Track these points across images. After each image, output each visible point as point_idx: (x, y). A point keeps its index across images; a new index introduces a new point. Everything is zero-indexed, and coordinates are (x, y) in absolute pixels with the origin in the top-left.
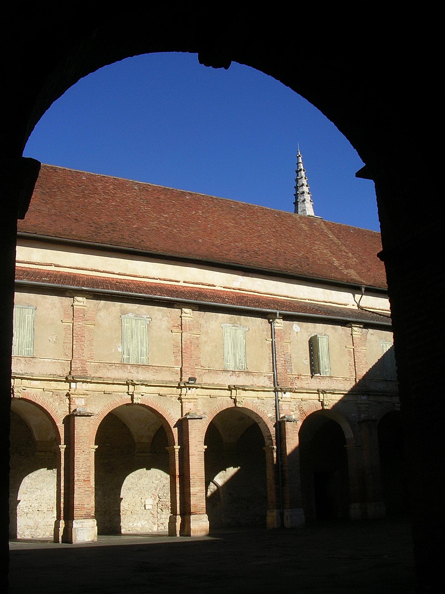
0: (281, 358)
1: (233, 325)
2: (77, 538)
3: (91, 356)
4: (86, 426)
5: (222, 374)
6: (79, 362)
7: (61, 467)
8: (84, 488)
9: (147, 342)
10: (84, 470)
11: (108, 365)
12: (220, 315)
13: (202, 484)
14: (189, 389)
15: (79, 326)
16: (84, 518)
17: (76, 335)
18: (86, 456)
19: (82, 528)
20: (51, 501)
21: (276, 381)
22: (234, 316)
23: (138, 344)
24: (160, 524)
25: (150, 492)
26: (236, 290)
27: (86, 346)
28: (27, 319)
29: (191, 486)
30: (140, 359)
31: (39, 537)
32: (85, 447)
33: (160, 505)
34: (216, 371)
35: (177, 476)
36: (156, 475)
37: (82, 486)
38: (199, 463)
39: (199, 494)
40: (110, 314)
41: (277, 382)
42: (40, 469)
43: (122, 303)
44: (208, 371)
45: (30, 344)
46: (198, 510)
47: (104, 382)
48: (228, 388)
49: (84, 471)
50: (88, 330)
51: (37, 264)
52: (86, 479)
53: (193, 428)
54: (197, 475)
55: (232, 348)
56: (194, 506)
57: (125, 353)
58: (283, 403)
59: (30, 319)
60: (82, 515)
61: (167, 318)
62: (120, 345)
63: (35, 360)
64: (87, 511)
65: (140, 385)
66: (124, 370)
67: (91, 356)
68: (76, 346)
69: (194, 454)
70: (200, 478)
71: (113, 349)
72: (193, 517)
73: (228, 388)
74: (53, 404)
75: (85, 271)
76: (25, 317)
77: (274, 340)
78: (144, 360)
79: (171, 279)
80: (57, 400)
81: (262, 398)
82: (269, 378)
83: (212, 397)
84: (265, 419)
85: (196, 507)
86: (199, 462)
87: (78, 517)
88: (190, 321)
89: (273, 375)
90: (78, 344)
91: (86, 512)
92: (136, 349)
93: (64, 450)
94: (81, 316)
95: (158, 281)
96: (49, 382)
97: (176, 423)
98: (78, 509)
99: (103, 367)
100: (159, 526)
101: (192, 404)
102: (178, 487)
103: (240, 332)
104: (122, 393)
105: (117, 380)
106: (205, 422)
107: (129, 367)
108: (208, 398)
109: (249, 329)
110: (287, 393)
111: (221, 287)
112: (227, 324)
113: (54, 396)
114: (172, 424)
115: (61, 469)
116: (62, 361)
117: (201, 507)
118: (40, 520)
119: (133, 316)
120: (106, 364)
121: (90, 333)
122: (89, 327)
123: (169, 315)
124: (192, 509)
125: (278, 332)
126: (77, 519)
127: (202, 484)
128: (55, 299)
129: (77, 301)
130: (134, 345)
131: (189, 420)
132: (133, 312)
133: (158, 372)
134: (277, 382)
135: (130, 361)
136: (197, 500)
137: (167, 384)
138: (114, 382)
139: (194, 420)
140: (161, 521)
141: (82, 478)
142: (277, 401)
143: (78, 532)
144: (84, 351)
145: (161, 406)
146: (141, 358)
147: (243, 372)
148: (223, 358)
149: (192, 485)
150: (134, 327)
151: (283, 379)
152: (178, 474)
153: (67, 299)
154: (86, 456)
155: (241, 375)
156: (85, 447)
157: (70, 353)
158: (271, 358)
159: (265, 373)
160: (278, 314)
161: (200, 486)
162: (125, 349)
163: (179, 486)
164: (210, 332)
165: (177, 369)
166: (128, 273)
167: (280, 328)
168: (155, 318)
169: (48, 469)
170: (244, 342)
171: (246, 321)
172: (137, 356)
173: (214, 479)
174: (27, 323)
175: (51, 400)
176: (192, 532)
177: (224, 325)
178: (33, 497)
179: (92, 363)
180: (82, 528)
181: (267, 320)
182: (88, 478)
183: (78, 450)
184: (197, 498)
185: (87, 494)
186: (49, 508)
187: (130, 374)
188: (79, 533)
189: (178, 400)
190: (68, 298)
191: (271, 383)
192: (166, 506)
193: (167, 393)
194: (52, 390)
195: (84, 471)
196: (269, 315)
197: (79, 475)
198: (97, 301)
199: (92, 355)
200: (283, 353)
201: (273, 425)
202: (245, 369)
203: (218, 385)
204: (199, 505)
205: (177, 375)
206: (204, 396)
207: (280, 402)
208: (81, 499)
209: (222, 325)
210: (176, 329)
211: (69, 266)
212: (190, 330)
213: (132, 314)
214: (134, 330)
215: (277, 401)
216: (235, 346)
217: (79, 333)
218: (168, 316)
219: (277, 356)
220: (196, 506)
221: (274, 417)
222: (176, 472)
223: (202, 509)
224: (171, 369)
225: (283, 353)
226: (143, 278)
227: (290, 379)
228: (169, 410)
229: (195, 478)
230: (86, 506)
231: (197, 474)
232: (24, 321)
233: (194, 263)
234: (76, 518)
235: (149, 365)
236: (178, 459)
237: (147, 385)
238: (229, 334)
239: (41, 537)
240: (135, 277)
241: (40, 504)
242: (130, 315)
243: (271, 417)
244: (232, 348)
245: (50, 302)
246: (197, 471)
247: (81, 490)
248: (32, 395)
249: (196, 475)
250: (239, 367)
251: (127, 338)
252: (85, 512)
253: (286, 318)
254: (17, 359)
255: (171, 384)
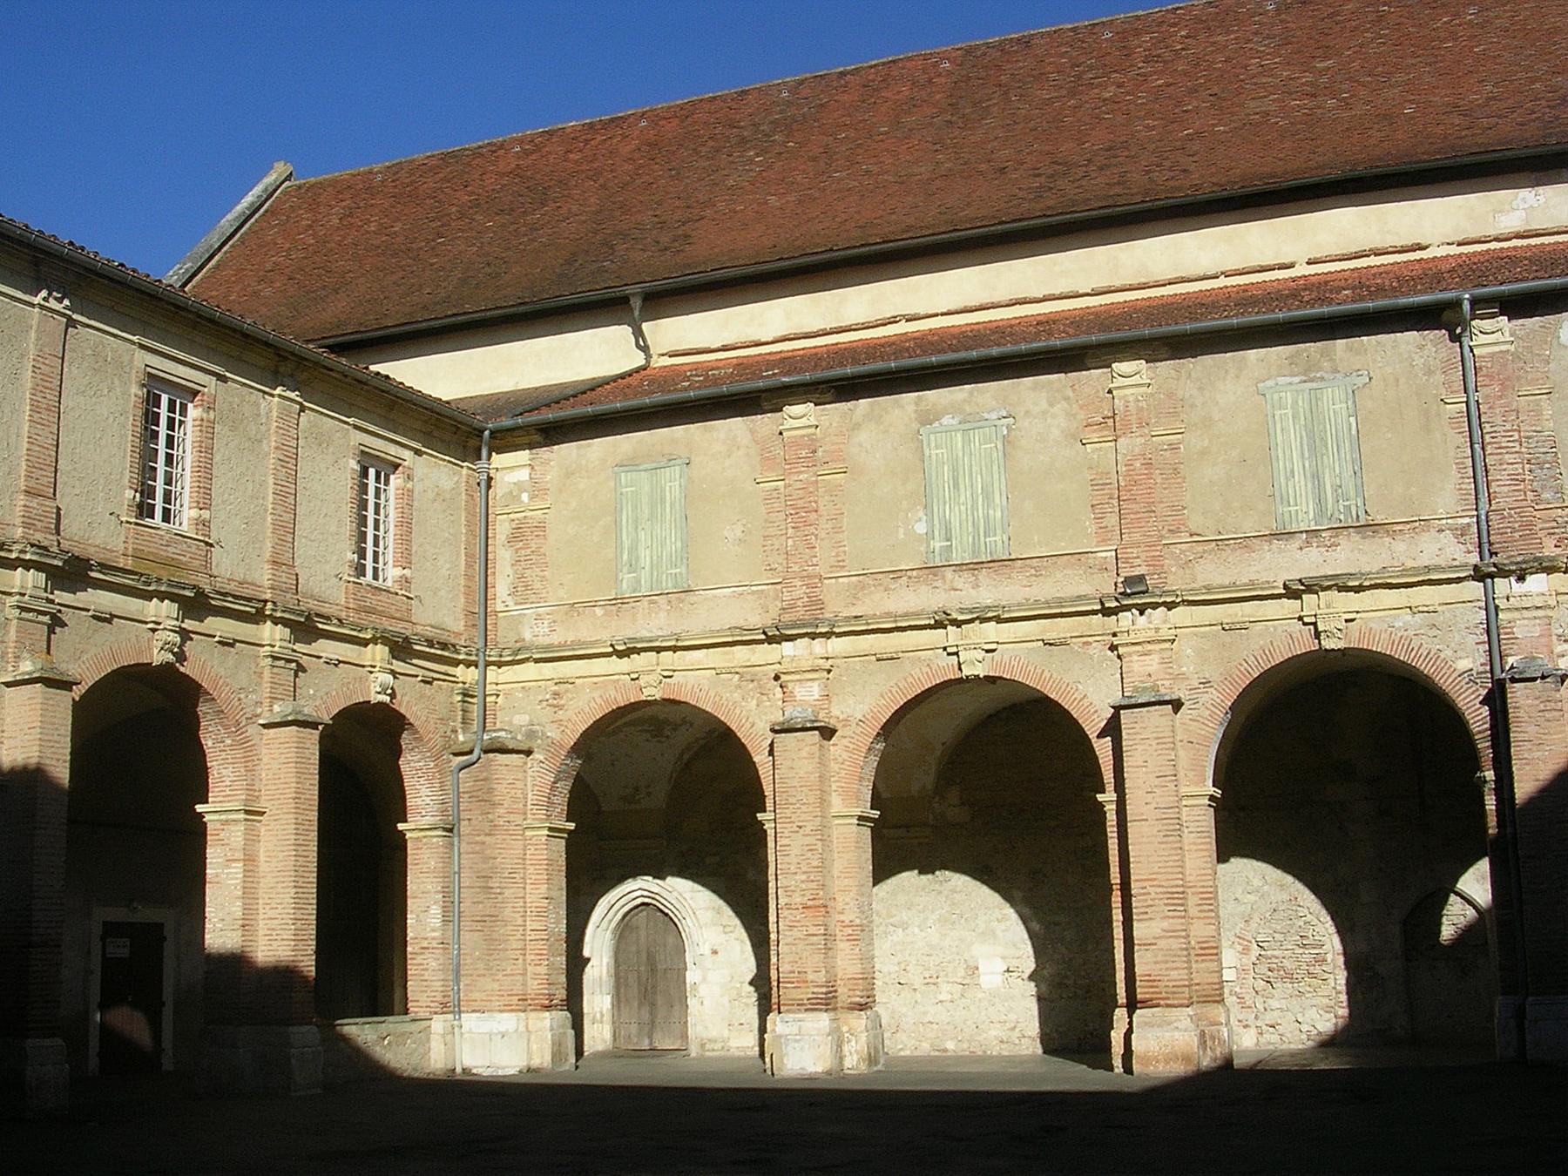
0: (1507, 456)
1: (1304, 378)
2: (785, 1062)
3: (839, 561)
4: (805, 758)
5: (1266, 548)
6: (800, 583)
7: (770, 872)
8: (804, 928)
9: (1004, 488)
10: (804, 877)
11: (886, 579)
12: (1253, 355)
13: (1175, 910)
14: (1142, 613)
15: (799, 485)
16: (806, 1010)
17: (793, 512)
18: (808, 840)
19: (798, 1037)
20: (933, 958)
21: (1485, 540)
22: (1308, 345)
23: (975, 502)
24: (1264, 1027)
25: (1229, 930)
26: (1510, 239)
27: (823, 534)
28: (668, 494)
29: (1135, 917)
30: (982, 543)
31: (902, 1053)
32: (804, 817)
33: (1263, 969)
34: (1244, 542)
35: (1114, 887)
36: (1247, 877)
37: (799, 921)
38: (1163, 846)
39: (1162, 943)
40: (887, 431)
41: (1490, 544)
42: (900, 872)
43: (921, 393)
44: (1214, 543)
45: (679, 559)
46: (1161, 993)
47: (870, 627)
48: (1284, 592)
49: (803, 882)
50: (826, 491)
51: (859, 326)
52: (810, 903)
53: (1139, 737)
54: (1155, 883)
55: (1306, 455)
56: (1148, 981)
57: (936, 533)
58: (1516, 615)
59: (677, 492)
60: (802, 1000)
61: (1066, 405)
62: (921, 514)
63: (690, 597)
64: (815, 990)
65: (977, 622)
66: (935, 584)
67: (839, 561)
68: (794, 541)
69: (1144, 817)
70: (1165, 893)
71: (901, 531)
72: (1142, 1016)
73: (1284, 592)
74: (741, 706)
75: (992, 310)
76: (663, 490)
77: (1474, 397)
78: (997, 545)
79: (1263, 264)
80: (751, 693)
81: (1426, 609)
82: (1462, 532)
83: (1227, 627)
84: (1445, 682)
85: (1155, 984)
86: (1162, 843)
87: (789, 1005)
88: (1140, 398)
89: (1475, 519)
90: (798, 534)
91: (813, 993)
92: (970, 518)
93: (1114, 807)
94: (804, 455)
95: (1222, 282)
96: (728, 648)
97: (1105, 721)
98: (789, 985)
99: (874, 585)
100: (1261, 1034)
101: (1156, 658)
102: (1117, 921)
103: (1334, 399)
104: (931, 652)
105: (906, 615)
106: (1208, 712)
107: (949, 573)
108: (1217, 631)
109: (1370, 379)
110: (1529, 578)
111: (1448, 244)
112: (1281, 380)
113: (745, 683)
114: (1092, 727)
115: (770, 878)
116: (760, 588)
117: (1171, 984)
118: (904, 1010)
119: (955, 422)
120: (880, 576)
121: (832, 498)
122: (829, 481)
123: (1071, 394)
124: (1138, 990)
125: (1489, 365)
126: (788, 1011)
127: (1175, 910)
128: (735, 426)
129: (790, 417)
130: (963, 508)
131: (1122, 712)
132: (954, 409)
133: (1041, 575)
134: (1490, 544)
135: (954, 555)
136: (1156, 963)
137: (1063, 607)
138: (899, 624)
139: (1150, 708)
140: (1269, 1018)
141: (798, 900)
142: (1492, 610)
143: (787, 1045)
144: (817, 550)
145: (1055, 675)
146: (988, 540)
147: (1351, 530)
148: (1269, 493)
149: (1138, 914)
150: (960, 454)
151: (1514, 530)
152: (1119, 882)
153: (766, 419)
154: (808, 840)
155: (1342, 540)
156: (804, 817)
157: (780, 561)
158: (1469, 462)
159: (1439, 519)
160: (1466, 306)
161: (1168, 917)
162: (936, 522)
163: (1121, 918)
164: (1216, 416)
165: (1104, 554)
166: (1118, 283)
167: (1496, 349)
168: (1027, 412)
169: (920, 873)
170: (1354, 425)
171: (1358, 353)
172: (974, 539)
173: (1458, 886)
174: (668, 505)
175: (736, 695)
176: (1137, 1062)
177: (1270, 383)
178: (884, 948)
179: (841, 580)
180: (798, 1037)
181: (1444, 331)
182: (814, 899)
183: (785, 825)
184: (1156, 956)
185: (812, 944)
186: (927, 976)
187: (952, 592)
188: (789, 1048)
189: (1109, 652)
190: (769, 415)
191: (1469, 552)
192: (1282, 972)
193: (1069, 635)
194: (737, 670)
195: (803, 882)
196: (1445, 313)
197: (789, 892)
198: (849, 404)
199: (840, 559)
200: (1517, 437)
201: (1481, 698)
202: (1358, 516)
203: (1252, 584)
204: (1166, 978)
205: (1105, 575)
206: (1202, 629)
207: (1501, 616)
208: (798, 956)
209: (1260, 385)
210: (1095, 431)
211: (945, 310)
212: (1140, 426)
213: (953, 418)
214: (961, 462)
215: (1492, 610)
216: (1314, 444)
217: (800, 503)
218: (1067, 399)
219: (1489, 450)
220: (1154, 981)
221: (1481, 669)
222: (1112, 876)
223: (1175, 989)
224: (1083, 558)
225: (1517, 437)
226: (1170, 284)
227: (1556, 525)
228: (1080, 687)
229: (1149, 894)
230: (811, 977)
231: (1155, 879)
232: (663, 500)
233: (1337, 194)
234: (786, 1008)
235: (1013, 557)
236: (1115, 835)
237: (999, 620)
238: (1290, 412)
239: (908, 1053)
240: (1144, 288)
241: (903, 967)
242: (946, 420)
243: (1471, 670)
244: (1306, 455)
245: (722, 436)
246: (1156, 870)
247: (795, 933)
248: (689, 687)
249: (1150, 883)
250: (1336, 513)
251: (941, 490)
252: (807, 993)
253: (1517, 306)
254: (651, 602)
255: (1079, 605)
